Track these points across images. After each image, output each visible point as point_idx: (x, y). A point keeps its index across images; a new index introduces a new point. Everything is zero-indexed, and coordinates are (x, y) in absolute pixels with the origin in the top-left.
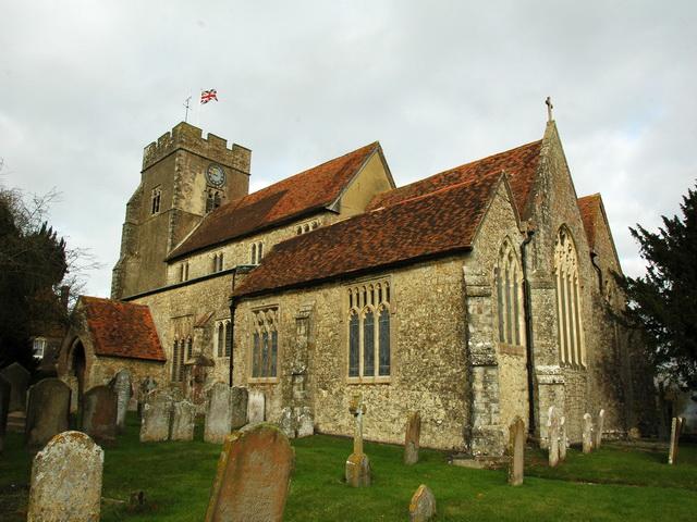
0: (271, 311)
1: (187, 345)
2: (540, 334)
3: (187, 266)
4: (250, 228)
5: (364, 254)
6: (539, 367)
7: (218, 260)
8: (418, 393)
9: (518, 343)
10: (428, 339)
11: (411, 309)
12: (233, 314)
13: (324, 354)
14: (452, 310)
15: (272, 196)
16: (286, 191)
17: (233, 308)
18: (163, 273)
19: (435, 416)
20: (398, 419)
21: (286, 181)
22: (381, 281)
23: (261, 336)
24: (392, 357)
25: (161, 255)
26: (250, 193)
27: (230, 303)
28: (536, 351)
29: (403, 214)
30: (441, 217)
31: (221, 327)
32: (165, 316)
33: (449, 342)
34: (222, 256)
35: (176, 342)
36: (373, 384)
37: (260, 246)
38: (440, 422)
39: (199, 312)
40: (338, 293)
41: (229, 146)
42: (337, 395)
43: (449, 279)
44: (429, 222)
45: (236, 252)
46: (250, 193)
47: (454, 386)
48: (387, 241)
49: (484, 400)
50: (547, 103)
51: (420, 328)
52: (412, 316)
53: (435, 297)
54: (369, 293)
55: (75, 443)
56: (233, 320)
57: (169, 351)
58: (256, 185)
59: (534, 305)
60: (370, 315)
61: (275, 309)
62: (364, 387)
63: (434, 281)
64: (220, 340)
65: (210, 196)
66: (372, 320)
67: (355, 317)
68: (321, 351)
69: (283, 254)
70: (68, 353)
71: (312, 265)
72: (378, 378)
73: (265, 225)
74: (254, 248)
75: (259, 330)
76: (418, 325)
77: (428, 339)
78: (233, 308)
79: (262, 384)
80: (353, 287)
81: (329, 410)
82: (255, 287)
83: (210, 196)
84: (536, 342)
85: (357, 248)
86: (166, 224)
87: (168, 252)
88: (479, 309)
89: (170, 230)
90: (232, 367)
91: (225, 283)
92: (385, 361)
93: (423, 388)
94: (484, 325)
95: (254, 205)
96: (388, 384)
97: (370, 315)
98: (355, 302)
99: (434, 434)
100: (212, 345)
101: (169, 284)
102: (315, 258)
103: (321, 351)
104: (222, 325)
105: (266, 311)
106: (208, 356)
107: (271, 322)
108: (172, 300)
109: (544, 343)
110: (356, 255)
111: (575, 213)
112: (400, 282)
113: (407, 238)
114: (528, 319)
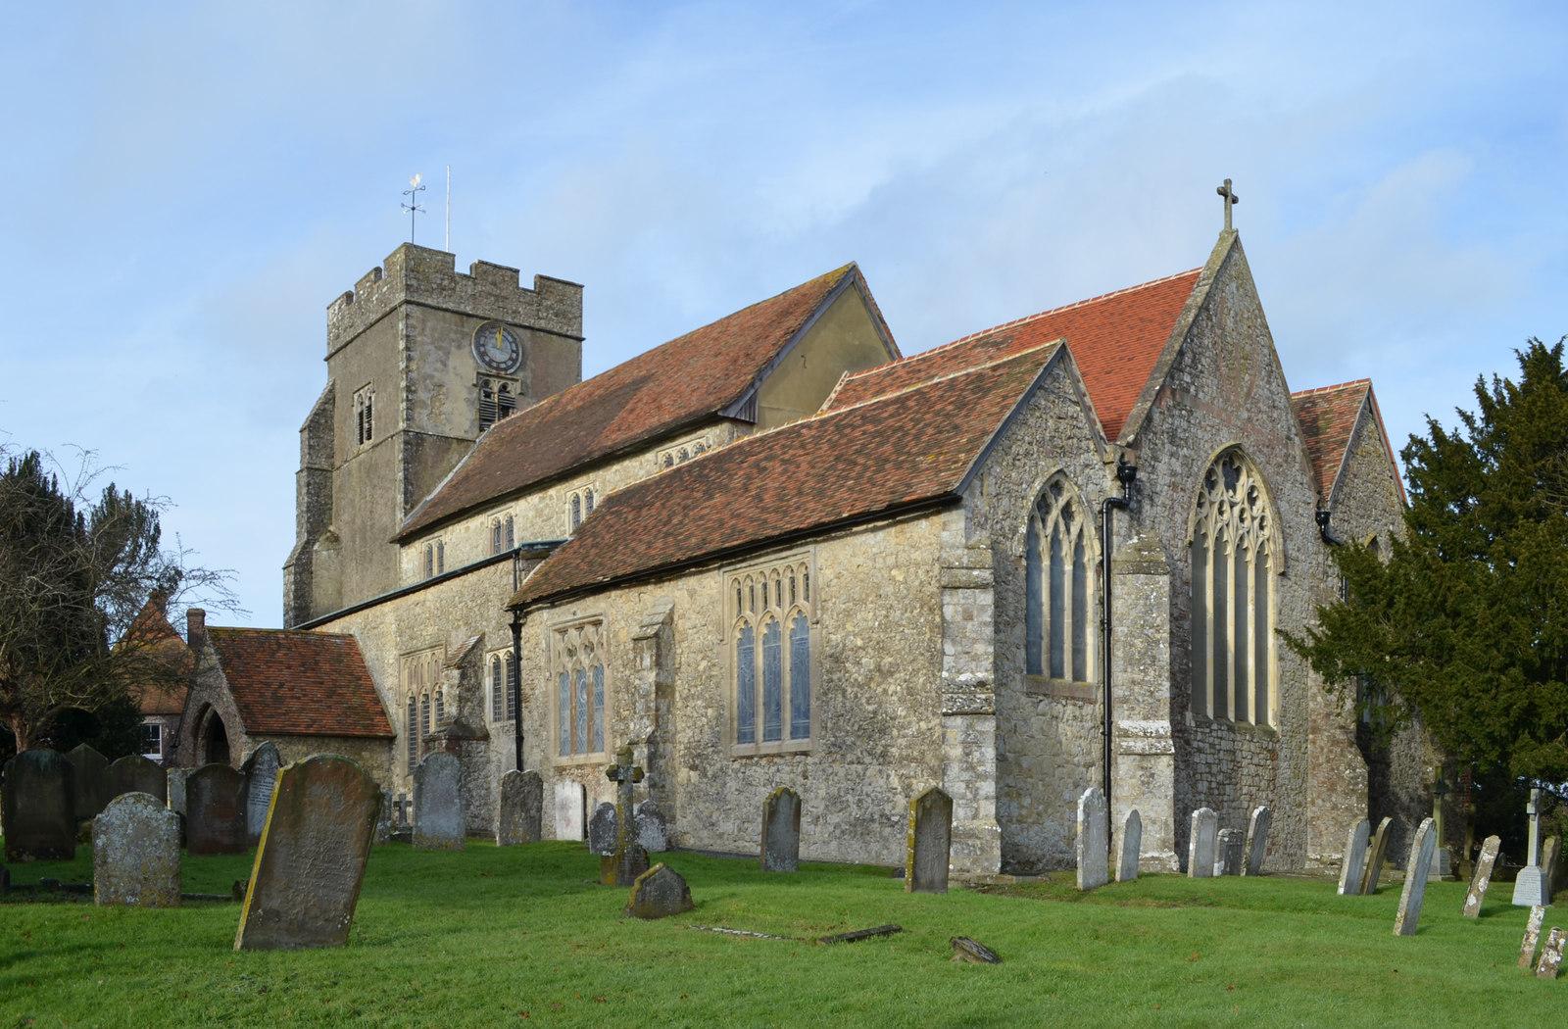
0: (590, 629)
1: (433, 705)
2: (1130, 661)
3: (441, 548)
4: (566, 458)
5: (764, 510)
6: (1122, 722)
7: (503, 532)
8: (860, 768)
9: (1079, 674)
10: (879, 669)
11: (848, 614)
12: (517, 638)
13: (691, 703)
14: (921, 614)
15: (627, 384)
16: (644, 380)
17: (516, 628)
18: (392, 566)
19: (888, 808)
20: (825, 816)
21: (652, 354)
22: (793, 562)
23: (573, 676)
24: (814, 704)
25: (385, 530)
26: (587, 374)
27: (510, 618)
28: (1118, 692)
29: (854, 428)
30: (917, 437)
31: (497, 666)
32: (398, 649)
33: (915, 672)
34: (510, 521)
35: (413, 698)
36: (780, 755)
37: (590, 497)
38: (895, 819)
39: (453, 639)
40: (713, 585)
41: (527, 282)
42: (715, 777)
43: (916, 555)
44: (894, 445)
45: (539, 513)
46: (587, 374)
47: (923, 753)
48: (811, 483)
49: (966, 776)
50: (1224, 192)
51: (863, 648)
52: (849, 627)
53: (890, 589)
54: (772, 586)
55: (140, 806)
56: (518, 648)
57: (398, 715)
58: (598, 358)
59: (1118, 606)
60: (774, 626)
61: (597, 623)
62: (764, 762)
63: (891, 561)
64: (497, 688)
65: (488, 395)
66: (751, 640)
67: (747, 631)
68: (686, 699)
69: (618, 514)
70: (195, 737)
71: (667, 535)
72: (789, 744)
73: (596, 455)
74: (577, 502)
75: (570, 666)
76: (859, 643)
77: (879, 669)
78: (516, 628)
79: (579, 767)
80: (741, 574)
81: (701, 806)
82: (559, 579)
83: (488, 395)
84: (1119, 677)
85: (754, 497)
86: (389, 463)
87: (400, 521)
88: (965, 611)
89: (400, 475)
90: (520, 740)
91: (501, 581)
92: (802, 712)
93: (868, 759)
94: (975, 641)
95: (580, 409)
96: (805, 754)
97: (774, 626)
98: (747, 604)
99: (886, 839)
100: (481, 701)
101: (406, 584)
102: (675, 521)
103: (686, 699)
104: (498, 659)
105: (580, 628)
106: (474, 724)
107: (589, 647)
108: (399, 620)
109: (1138, 677)
110: (753, 512)
111: (1287, 422)
112: (828, 559)
113: (847, 478)
114: (1106, 627)
